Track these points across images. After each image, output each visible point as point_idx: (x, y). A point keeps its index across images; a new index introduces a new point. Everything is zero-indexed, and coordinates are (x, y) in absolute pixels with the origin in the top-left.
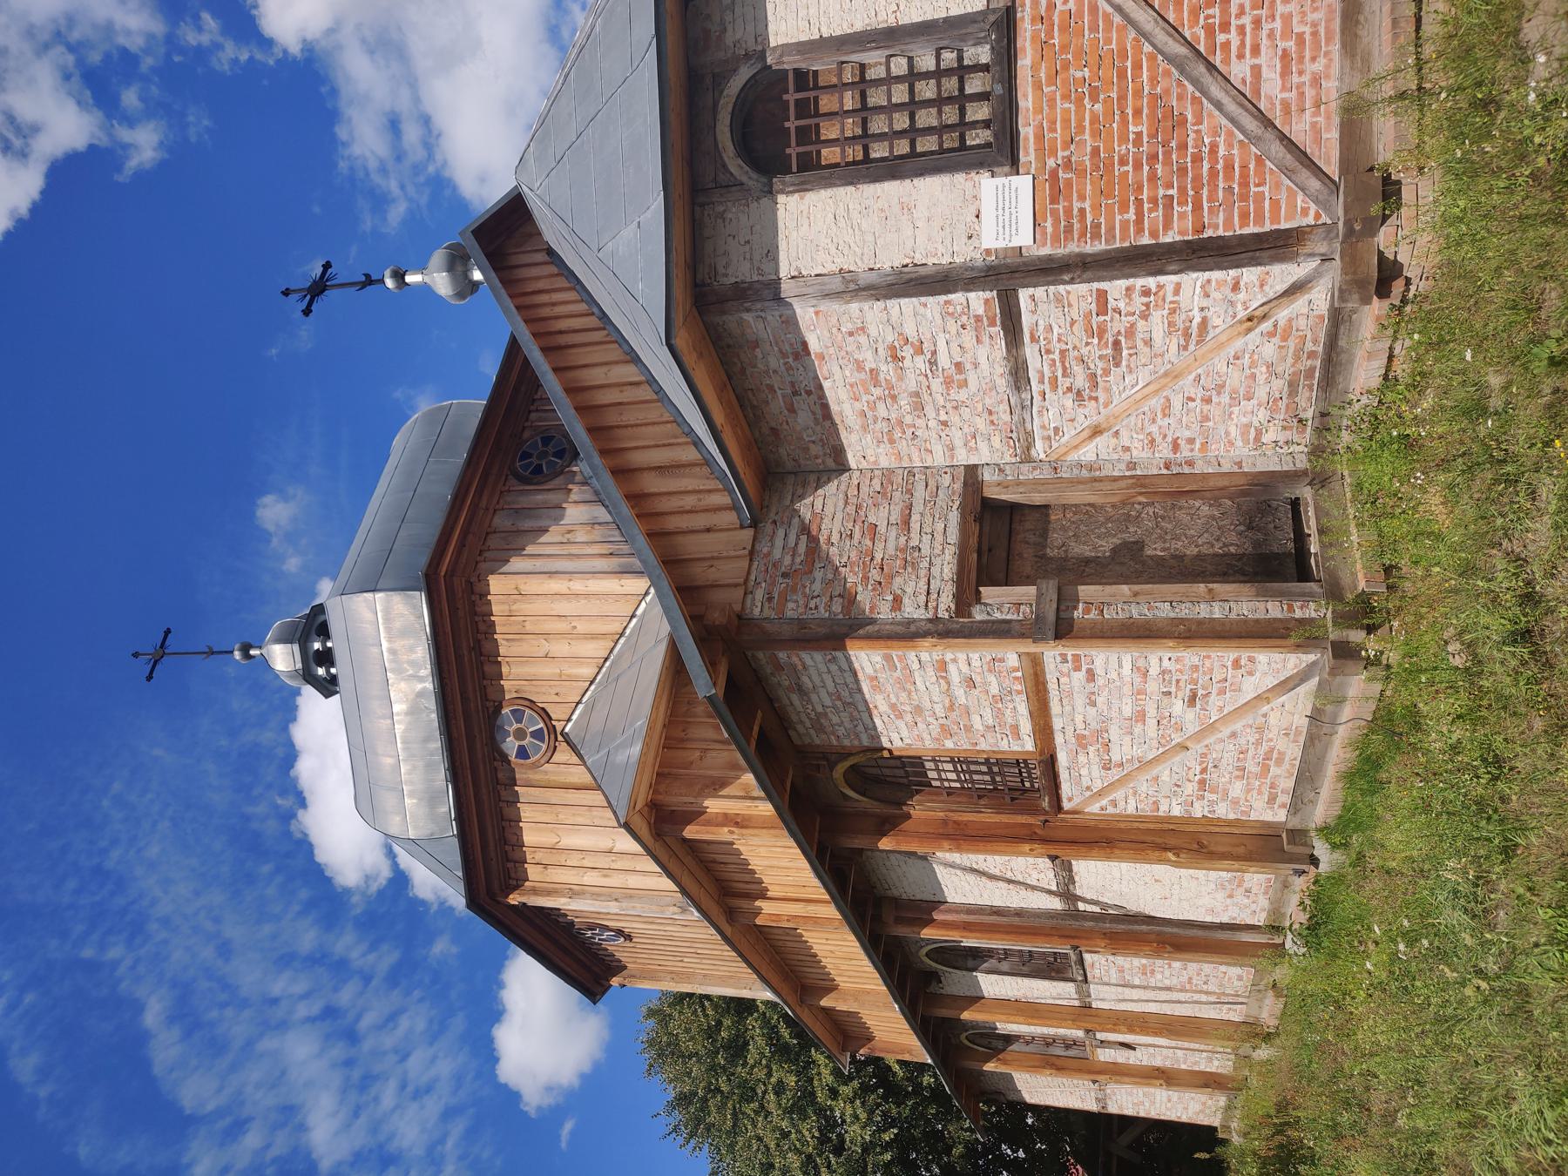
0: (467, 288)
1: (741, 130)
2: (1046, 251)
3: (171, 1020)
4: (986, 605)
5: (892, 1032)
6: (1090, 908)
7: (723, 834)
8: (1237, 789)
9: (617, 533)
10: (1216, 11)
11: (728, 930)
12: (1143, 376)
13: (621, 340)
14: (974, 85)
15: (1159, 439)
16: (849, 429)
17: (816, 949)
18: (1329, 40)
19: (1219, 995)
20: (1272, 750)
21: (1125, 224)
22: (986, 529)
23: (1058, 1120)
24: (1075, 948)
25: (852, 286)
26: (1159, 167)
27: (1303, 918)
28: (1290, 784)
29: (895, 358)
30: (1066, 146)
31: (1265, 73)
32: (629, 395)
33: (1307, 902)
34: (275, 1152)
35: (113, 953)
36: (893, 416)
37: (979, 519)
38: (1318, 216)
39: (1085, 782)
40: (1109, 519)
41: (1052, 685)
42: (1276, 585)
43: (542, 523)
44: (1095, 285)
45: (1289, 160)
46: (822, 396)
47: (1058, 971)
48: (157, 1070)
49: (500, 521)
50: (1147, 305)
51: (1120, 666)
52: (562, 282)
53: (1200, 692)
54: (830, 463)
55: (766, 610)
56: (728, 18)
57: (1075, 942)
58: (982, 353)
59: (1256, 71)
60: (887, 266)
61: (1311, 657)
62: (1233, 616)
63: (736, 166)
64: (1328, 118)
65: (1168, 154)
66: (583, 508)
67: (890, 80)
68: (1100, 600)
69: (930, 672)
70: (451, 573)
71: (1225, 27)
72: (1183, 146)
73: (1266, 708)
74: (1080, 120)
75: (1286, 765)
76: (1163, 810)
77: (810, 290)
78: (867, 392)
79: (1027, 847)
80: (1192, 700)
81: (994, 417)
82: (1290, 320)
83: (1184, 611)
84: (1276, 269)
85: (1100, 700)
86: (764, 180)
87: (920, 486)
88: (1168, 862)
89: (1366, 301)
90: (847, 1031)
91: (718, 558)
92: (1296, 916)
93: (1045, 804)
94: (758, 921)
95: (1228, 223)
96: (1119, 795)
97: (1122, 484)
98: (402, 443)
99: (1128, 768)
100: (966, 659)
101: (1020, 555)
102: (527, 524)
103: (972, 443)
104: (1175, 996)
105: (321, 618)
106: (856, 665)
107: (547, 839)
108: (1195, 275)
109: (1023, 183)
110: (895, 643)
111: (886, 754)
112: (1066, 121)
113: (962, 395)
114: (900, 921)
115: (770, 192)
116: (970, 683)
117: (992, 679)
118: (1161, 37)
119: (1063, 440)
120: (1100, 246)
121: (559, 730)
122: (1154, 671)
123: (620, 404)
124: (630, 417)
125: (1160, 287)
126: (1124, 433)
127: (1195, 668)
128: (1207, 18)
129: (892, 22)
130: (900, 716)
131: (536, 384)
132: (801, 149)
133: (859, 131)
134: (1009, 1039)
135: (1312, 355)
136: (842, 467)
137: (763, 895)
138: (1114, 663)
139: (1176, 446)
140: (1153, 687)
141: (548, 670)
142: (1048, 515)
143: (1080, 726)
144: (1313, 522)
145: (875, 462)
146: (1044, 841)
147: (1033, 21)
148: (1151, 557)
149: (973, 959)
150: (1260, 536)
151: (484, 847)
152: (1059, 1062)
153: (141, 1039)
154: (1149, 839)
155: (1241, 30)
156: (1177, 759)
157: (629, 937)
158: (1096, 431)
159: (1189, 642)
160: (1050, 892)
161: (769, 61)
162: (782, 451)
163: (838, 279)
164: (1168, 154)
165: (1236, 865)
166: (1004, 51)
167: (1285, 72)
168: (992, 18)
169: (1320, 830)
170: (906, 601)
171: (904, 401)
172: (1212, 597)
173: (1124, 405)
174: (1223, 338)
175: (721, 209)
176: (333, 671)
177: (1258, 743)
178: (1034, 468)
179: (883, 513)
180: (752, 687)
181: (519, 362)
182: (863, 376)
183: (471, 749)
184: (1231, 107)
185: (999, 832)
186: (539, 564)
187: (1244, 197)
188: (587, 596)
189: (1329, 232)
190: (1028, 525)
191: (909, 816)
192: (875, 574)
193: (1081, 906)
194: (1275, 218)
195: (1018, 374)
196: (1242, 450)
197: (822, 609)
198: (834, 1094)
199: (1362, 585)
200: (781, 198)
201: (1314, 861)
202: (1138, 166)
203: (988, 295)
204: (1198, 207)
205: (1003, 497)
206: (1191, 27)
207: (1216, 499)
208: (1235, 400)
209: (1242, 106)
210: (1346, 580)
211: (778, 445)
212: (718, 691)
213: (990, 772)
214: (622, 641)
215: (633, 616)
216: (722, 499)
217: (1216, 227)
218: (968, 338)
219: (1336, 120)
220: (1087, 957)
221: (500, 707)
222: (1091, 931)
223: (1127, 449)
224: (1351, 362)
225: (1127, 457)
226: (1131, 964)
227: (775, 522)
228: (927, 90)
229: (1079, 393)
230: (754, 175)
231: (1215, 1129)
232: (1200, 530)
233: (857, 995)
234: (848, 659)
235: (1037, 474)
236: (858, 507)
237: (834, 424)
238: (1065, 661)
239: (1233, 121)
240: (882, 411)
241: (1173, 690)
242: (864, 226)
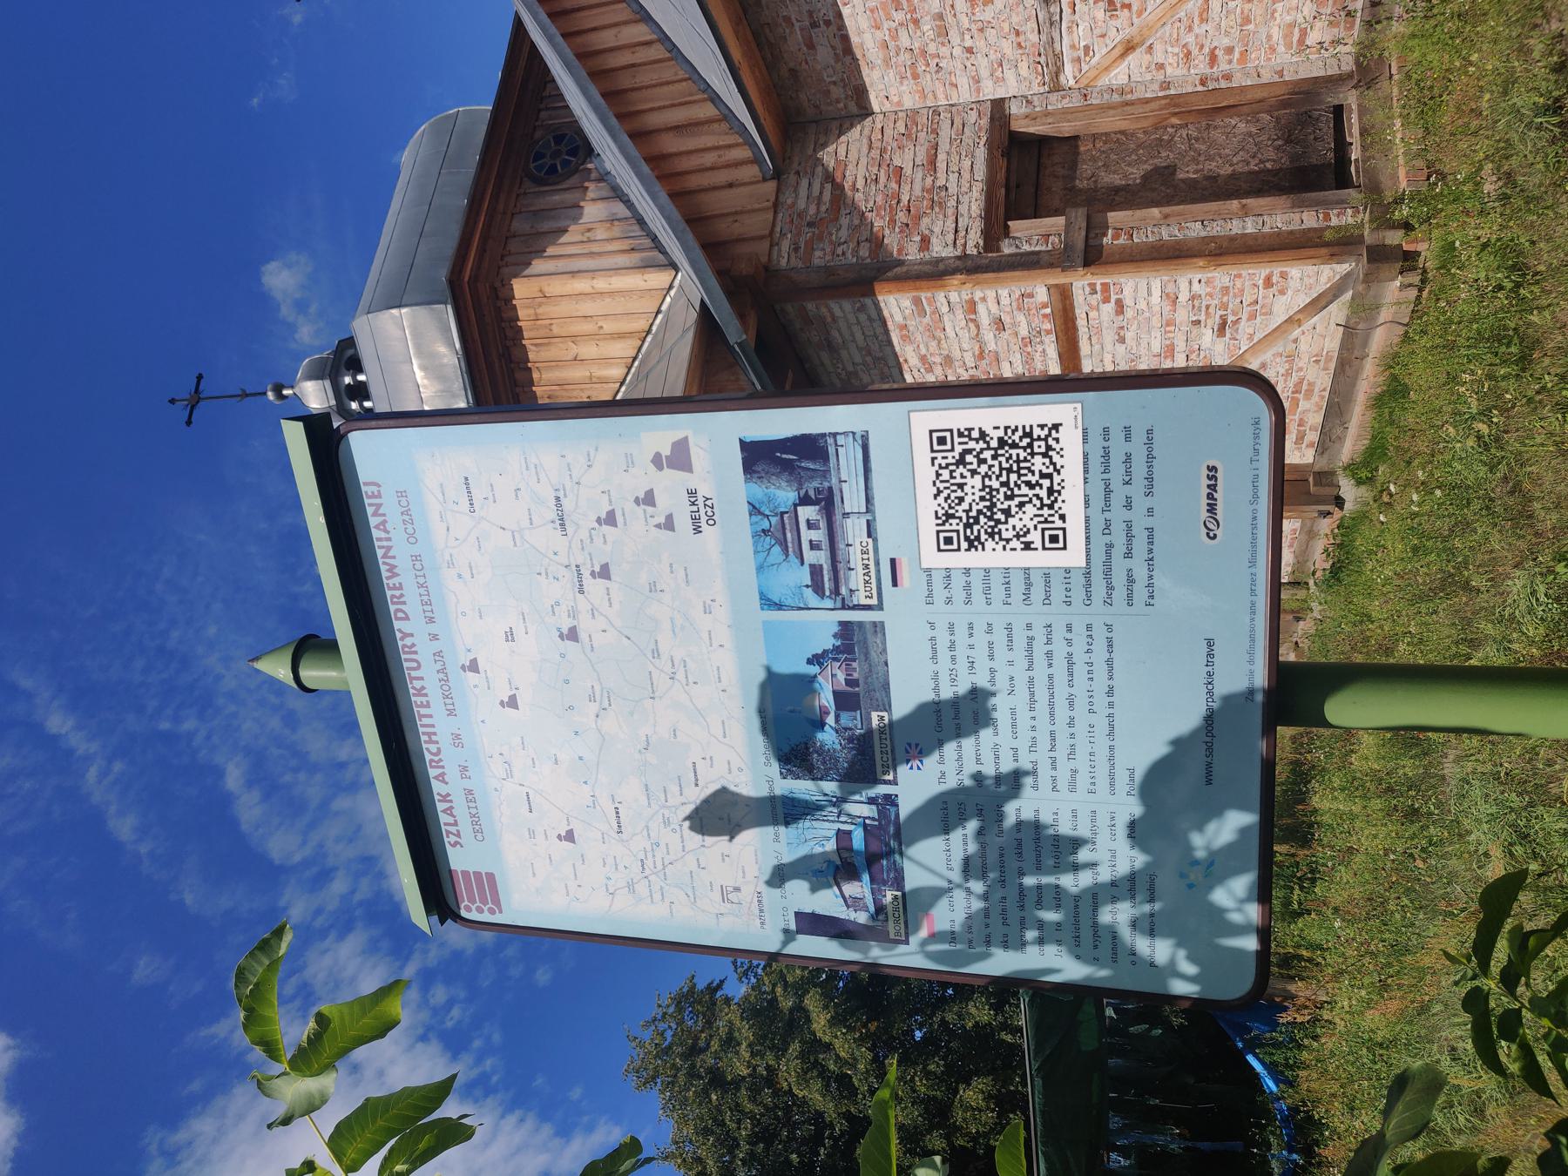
3: (250, 784)
9: (637, 227)
15: (1195, 52)
20: (1301, 382)
28: (1319, 419)
34: (358, 897)
35: (189, 725)
37: (1007, 154)
40: (1139, 146)
41: (1081, 322)
42: (1313, 195)
43: (561, 224)
46: (842, 27)
48: (244, 827)
49: (519, 225)
51: (1149, 294)
53: (1231, 318)
55: (793, 259)
61: (1345, 268)
62: (1266, 229)
66: (600, 205)
68: (1130, 225)
70: (475, 278)
73: (1297, 332)
75: (1315, 398)
80: (1222, 329)
81: (1021, 39)
83: (1216, 229)
85: (1129, 335)
91: (742, 212)
97: (1154, 105)
98: (412, 157)
100: (996, 296)
103: (998, 73)
105: (350, 352)
106: (886, 313)
110: (924, 284)
116: (999, 325)
117: (1021, 318)
119: (1094, 61)
122: (1183, 297)
123: (633, 65)
124: (644, 78)
126: (1158, 47)
131: (546, 70)
136: (865, 111)
138: (1141, 289)
139: (1213, 59)
140: (1183, 315)
141: (577, 373)
142: (1077, 147)
145: (899, 103)
150: (1299, 149)
153: (227, 800)
158: (1129, 47)
159: (1223, 259)
162: (802, 96)
170: (934, 240)
171: (927, 26)
172: (1245, 212)
176: (361, 378)
178: (1063, 97)
179: (909, 155)
181: (526, 49)
186: (561, 265)
188: (611, 293)
190: (1056, 159)
192: (901, 217)
201: (1339, 502)
205: (1031, 130)
210: (1385, 181)
212: (748, 337)
214: (649, 339)
215: (659, 312)
223: (1160, 67)
227: (798, 173)
232: (1237, 146)
235: (1066, 103)
236: (883, 151)
237: (855, 60)
238: (1094, 292)
241: (1202, 318)
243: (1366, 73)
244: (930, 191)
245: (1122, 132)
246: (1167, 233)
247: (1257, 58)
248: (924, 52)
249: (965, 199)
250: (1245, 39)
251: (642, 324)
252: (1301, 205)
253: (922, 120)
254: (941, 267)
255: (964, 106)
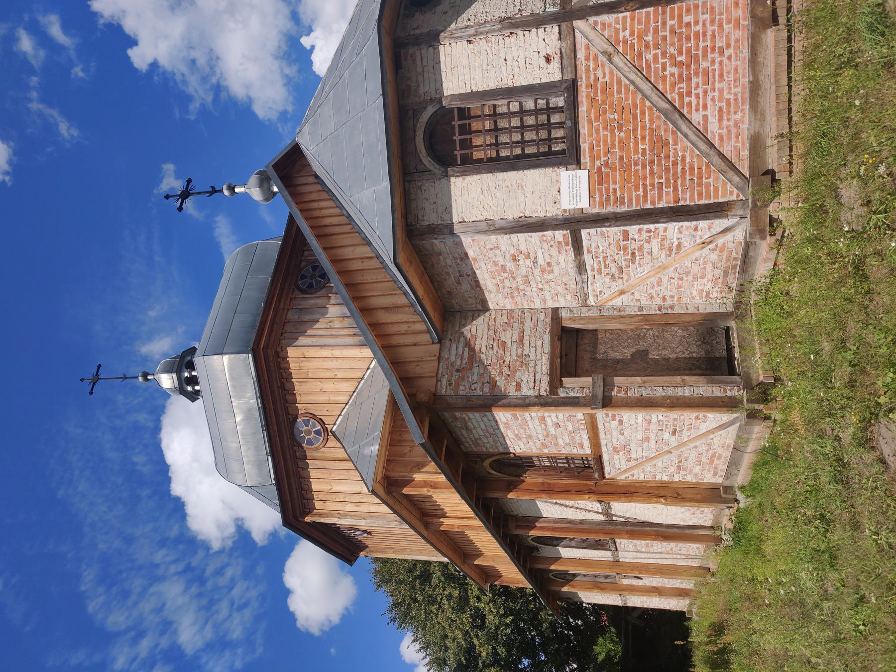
0: (269, 195)
1: (431, 139)
2: (596, 210)
4: (565, 388)
5: (511, 574)
6: (619, 519)
7: (424, 491)
8: (697, 469)
10: (684, 85)
11: (425, 533)
12: (647, 268)
13: (360, 232)
14: (556, 118)
15: (655, 296)
16: (490, 292)
17: (472, 538)
18: (743, 103)
19: (687, 555)
21: (638, 197)
22: (564, 343)
23: (598, 608)
24: (611, 539)
25: (492, 228)
26: (655, 167)
27: (730, 526)
29: (515, 260)
30: (606, 155)
31: (710, 119)
32: (367, 264)
33: (733, 518)
36: (514, 286)
38: (738, 196)
39: (618, 466)
41: (600, 427)
43: (316, 317)
44: (622, 228)
45: (723, 166)
47: (602, 545)
49: (292, 316)
50: (650, 237)
51: (636, 418)
52: (324, 196)
54: (479, 307)
56: (420, 79)
57: (612, 536)
58: (561, 258)
59: (706, 118)
60: (511, 218)
61: (735, 415)
62: (695, 394)
63: (427, 161)
64: (743, 144)
65: (659, 160)
66: (337, 308)
67: (511, 114)
68: (627, 385)
69: (537, 421)
70: (266, 347)
71: (689, 94)
72: (667, 157)
73: (712, 436)
74: (613, 141)
75: (723, 459)
76: (658, 478)
77: (469, 229)
78: (499, 275)
79: (587, 497)
80: (674, 433)
82: (724, 244)
83: (670, 392)
84: (717, 222)
85: (625, 433)
86: (443, 169)
87: (528, 320)
88: (661, 503)
89: (764, 238)
90: (488, 574)
91: (421, 361)
92: (727, 523)
93: (596, 475)
94: (441, 528)
95: (692, 197)
96: (635, 472)
99: (640, 461)
100: (554, 416)
101: (583, 358)
102: (307, 317)
104: (663, 556)
106: (497, 418)
107: (325, 487)
108: (674, 224)
109: (583, 174)
111: (512, 455)
112: (606, 141)
113: (551, 276)
114: (518, 527)
115: (447, 176)
116: (558, 425)
117: (569, 424)
118: (655, 98)
120: (624, 209)
121: (329, 430)
125: (656, 229)
127: (676, 420)
128: (679, 89)
129: (510, 84)
130: (520, 439)
132: (462, 137)
133: (493, 141)
134: (575, 575)
135: (735, 259)
136: (486, 309)
137: (444, 516)
138: (634, 418)
139: (664, 299)
140: (653, 427)
142: (596, 335)
143: (615, 443)
144: (736, 340)
146: (596, 493)
147: (587, 87)
148: (652, 359)
149: (554, 542)
150: (709, 348)
151: (291, 494)
152: (601, 585)
154: (651, 491)
155: (697, 96)
156: (666, 457)
157: (370, 533)
158: (622, 293)
160: (598, 513)
161: (444, 104)
162: (454, 302)
163: (484, 224)
164: (659, 160)
165: (697, 504)
166: (572, 103)
167: (721, 120)
168: (565, 85)
169: (741, 488)
170: (523, 385)
171: (519, 279)
172: (684, 384)
173: (637, 281)
174: (690, 251)
175: (420, 184)
176: (197, 388)
177: (708, 450)
178: (589, 310)
179: (509, 335)
180: (439, 424)
182: (497, 268)
183: (281, 441)
184: (693, 137)
185: (572, 489)
186: (315, 341)
187: (700, 185)
189: (744, 204)
190: (586, 341)
191: (524, 481)
192: (506, 370)
193: (614, 518)
194: (716, 197)
195: (581, 268)
196: (698, 301)
197: (478, 390)
198: (479, 599)
199: (761, 378)
200: (452, 179)
201: (737, 501)
202: (644, 166)
203: (565, 232)
204: (676, 189)
206: (671, 93)
207: (685, 327)
208: (695, 278)
209: (698, 136)
210: (754, 376)
211: (451, 301)
213: (568, 463)
214: (363, 382)
215: (368, 369)
216: (421, 327)
217: (686, 200)
218: (554, 251)
219: (747, 145)
220: (618, 541)
221: (296, 418)
222: (620, 530)
223: (639, 300)
224: (755, 262)
225: (638, 304)
226: (641, 544)
228: (530, 121)
229: (613, 275)
230: (437, 166)
231: (684, 612)
232: (678, 345)
233: (493, 558)
234: (493, 416)
235: (590, 313)
236: (495, 332)
237: (481, 289)
239: (693, 144)
240: (507, 283)
242: (498, 195)
243: (740, 310)
244: (520, 357)
245: (620, 330)
246: (645, 392)
247: (684, 301)
248: (517, 289)
249: (539, 363)
250: (680, 293)
251: (359, 374)
252: (711, 383)
253: (516, 316)
254: (527, 401)
255: (538, 309)
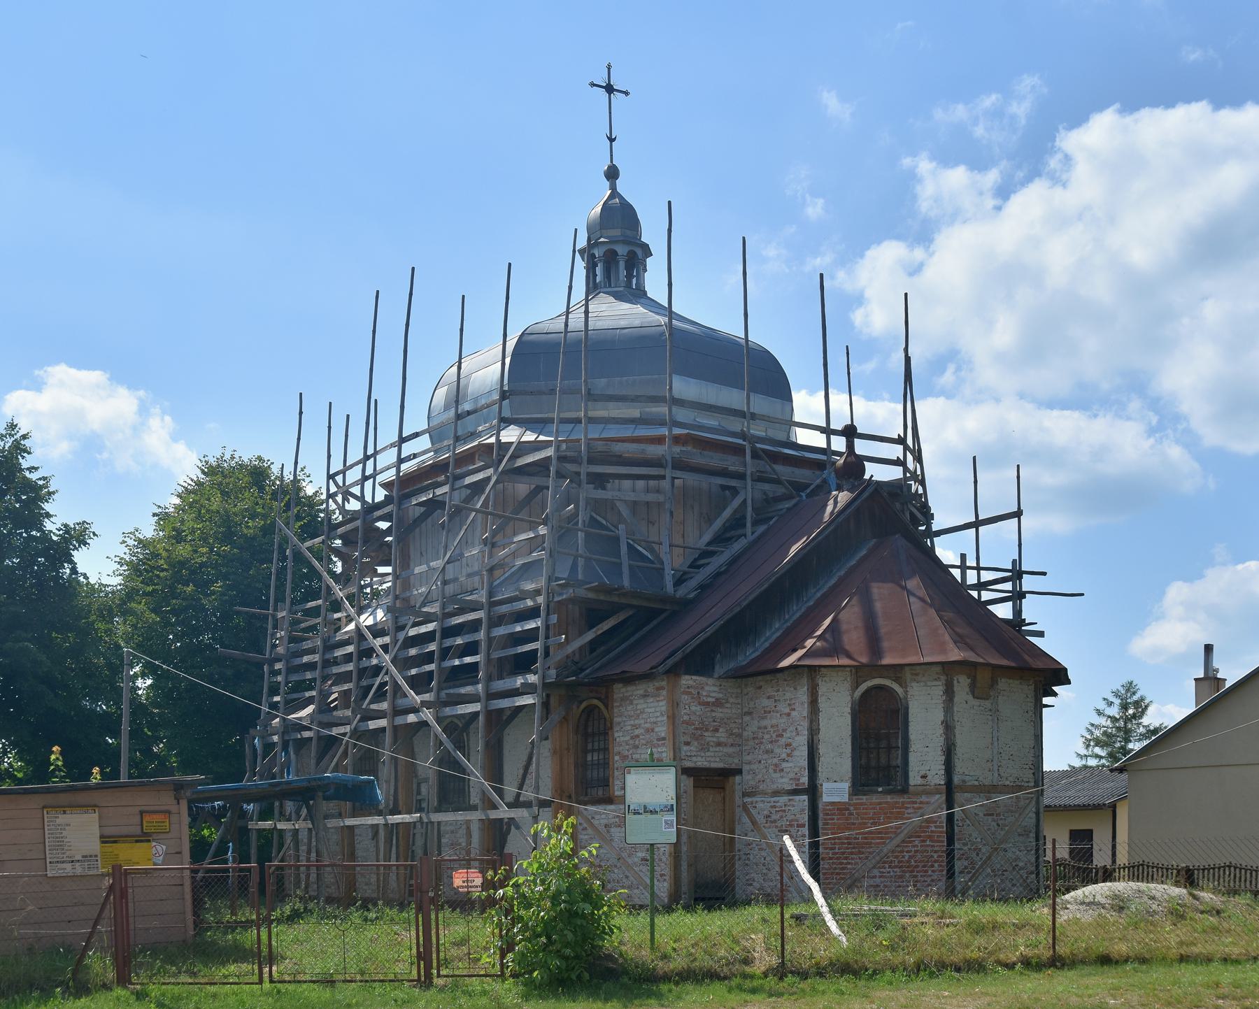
109: (845, 799)
113: (771, 771)
218: (792, 775)
